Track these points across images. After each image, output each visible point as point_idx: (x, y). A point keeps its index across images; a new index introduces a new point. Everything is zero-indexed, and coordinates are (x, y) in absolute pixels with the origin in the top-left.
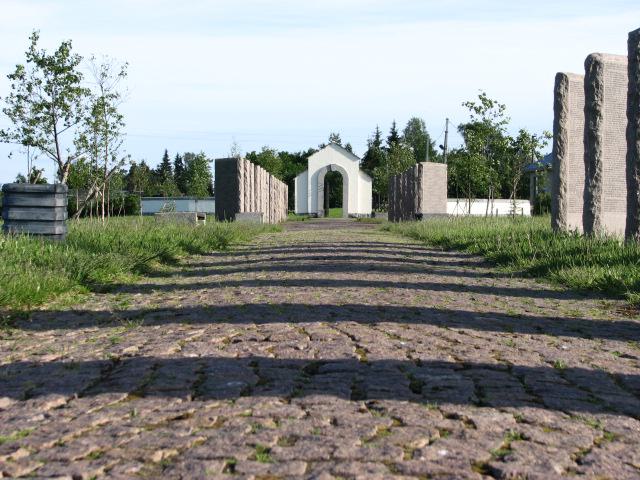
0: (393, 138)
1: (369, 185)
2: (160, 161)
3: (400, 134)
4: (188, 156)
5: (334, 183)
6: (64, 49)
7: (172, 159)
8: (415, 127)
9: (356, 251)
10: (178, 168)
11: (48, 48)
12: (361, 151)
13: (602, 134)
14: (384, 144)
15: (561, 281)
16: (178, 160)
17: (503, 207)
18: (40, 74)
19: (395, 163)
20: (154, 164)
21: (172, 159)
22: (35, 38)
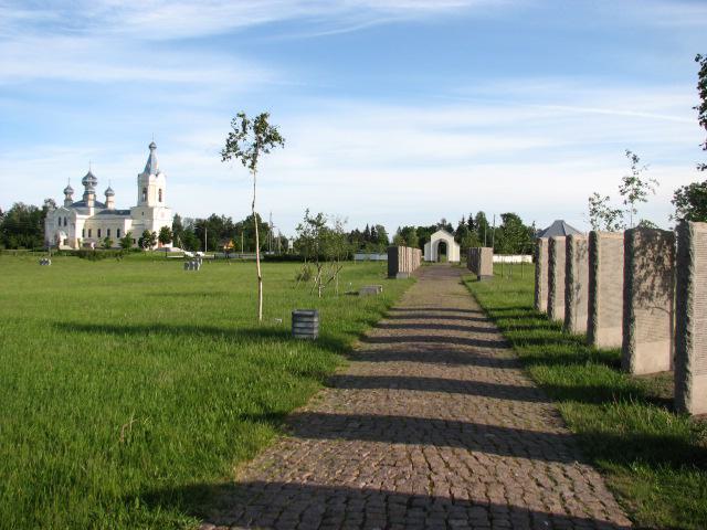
0: (471, 221)
1: (459, 248)
2: (364, 228)
3: (474, 218)
4: (378, 226)
5: (442, 248)
6: (319, 216)
7: (370, 228)
8: (481, 216)
9: (443, 317)
10: (373, 232)
11: (313, 216)
12: (455, 227)
13: (556, 272)
14: (466, 223)
15: (529, 375)
16: (373, 228)
17: (518, 259)
18: (310, 226)
19: (474, 233)
20: (362, 230)
21: (370, 228)
22: (308, 211)
